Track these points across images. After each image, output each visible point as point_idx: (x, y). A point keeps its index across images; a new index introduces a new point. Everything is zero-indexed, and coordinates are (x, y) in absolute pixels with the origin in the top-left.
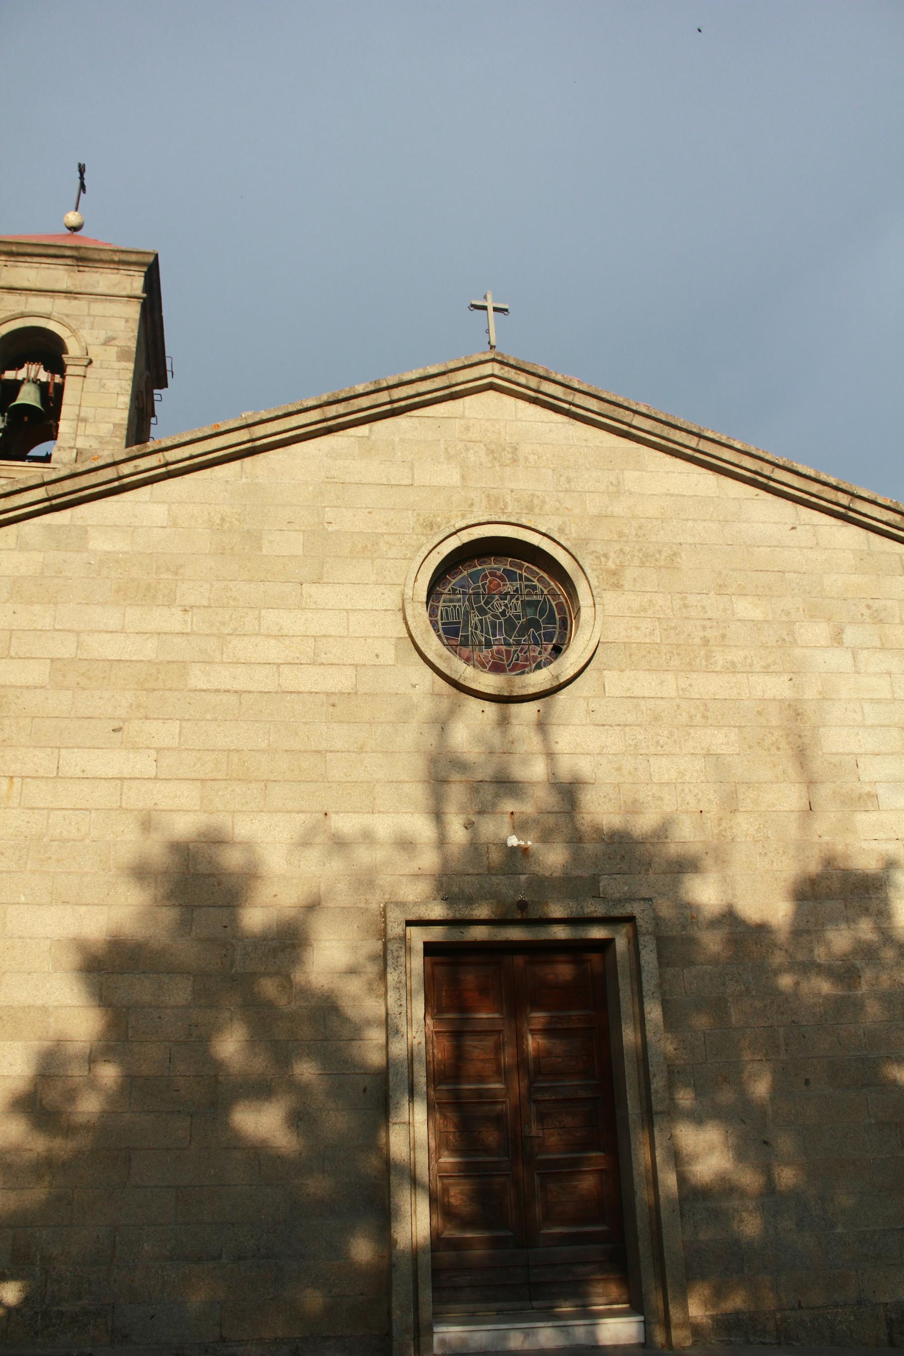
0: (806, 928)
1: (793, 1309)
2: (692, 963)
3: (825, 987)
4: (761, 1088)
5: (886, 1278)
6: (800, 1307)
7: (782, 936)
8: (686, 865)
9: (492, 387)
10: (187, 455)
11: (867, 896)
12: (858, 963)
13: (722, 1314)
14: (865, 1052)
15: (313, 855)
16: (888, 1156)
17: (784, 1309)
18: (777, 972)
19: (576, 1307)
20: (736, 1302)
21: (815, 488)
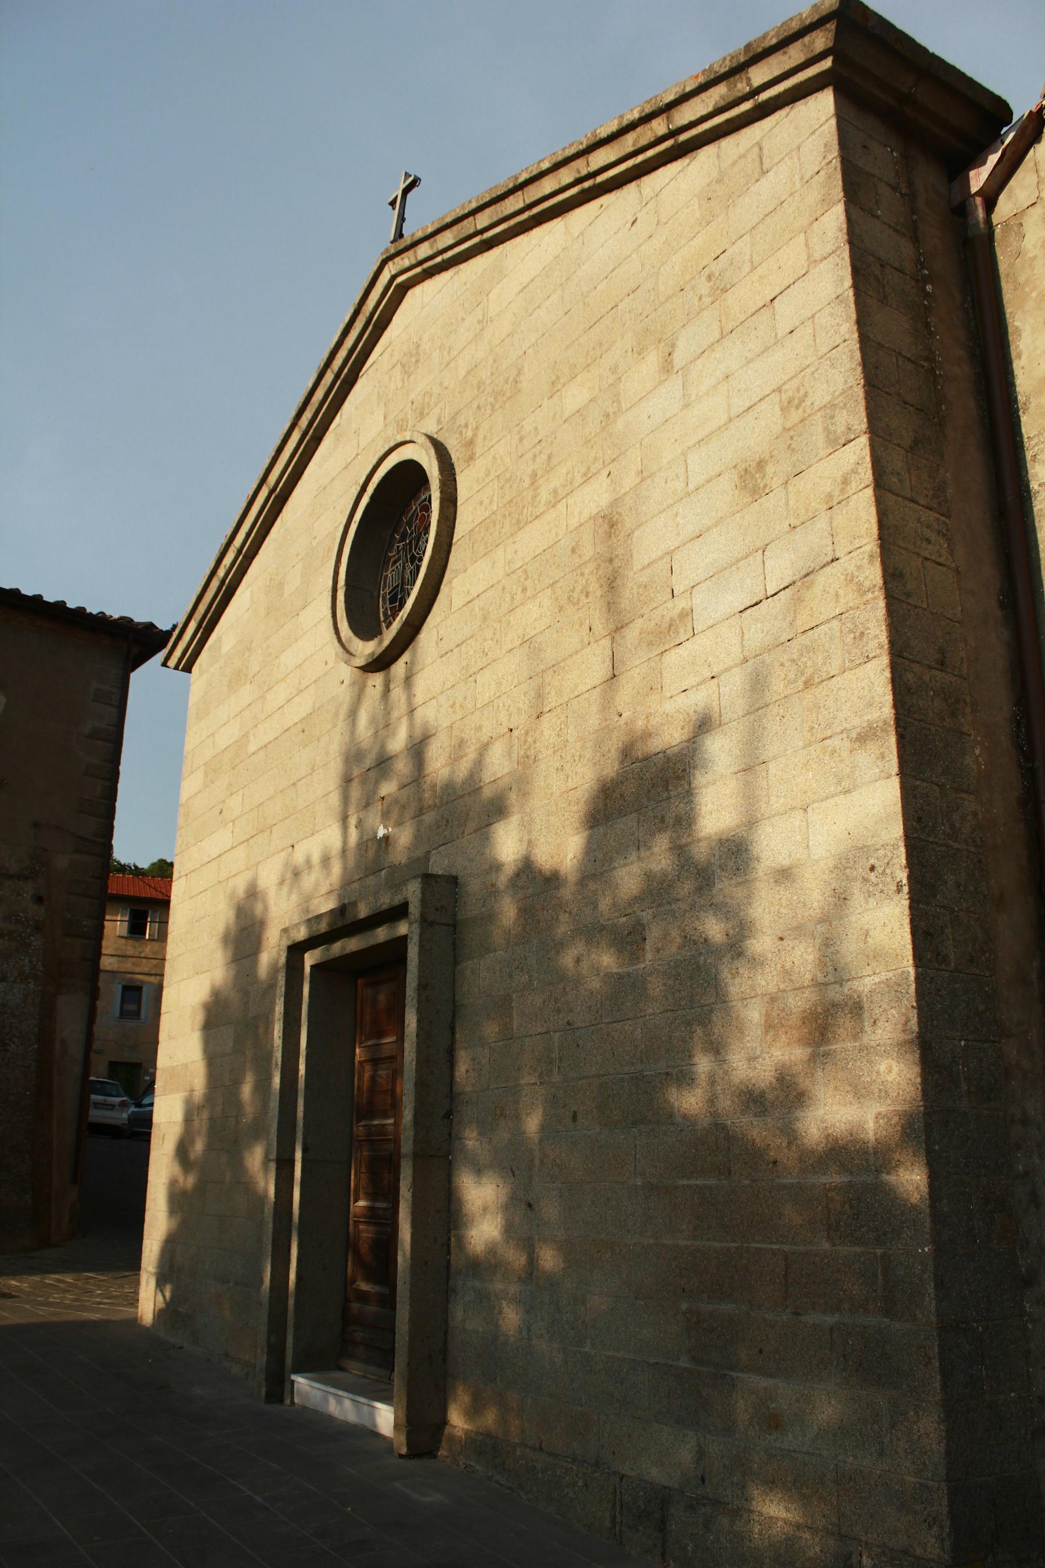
0: (597, 863)
1: (533, 1449)
2: (488, 950)
3: (608, 960)
4: (532, 1124)
5: (629, 1436)
6: (541, 1449)
7: (572, 878)
8: (497, 809)
9: (404, 289)
10: (521, 205)
11: (665, 795)
12: (646, 915)
13: (477, 1433)
14: (639, 1067)
15: (463, 423)
16: (652, 1241)
17: (526, 1446)
18: (560, 946)
19: (373, 1407)
20: (490, 1419)
21: (629, 142)
